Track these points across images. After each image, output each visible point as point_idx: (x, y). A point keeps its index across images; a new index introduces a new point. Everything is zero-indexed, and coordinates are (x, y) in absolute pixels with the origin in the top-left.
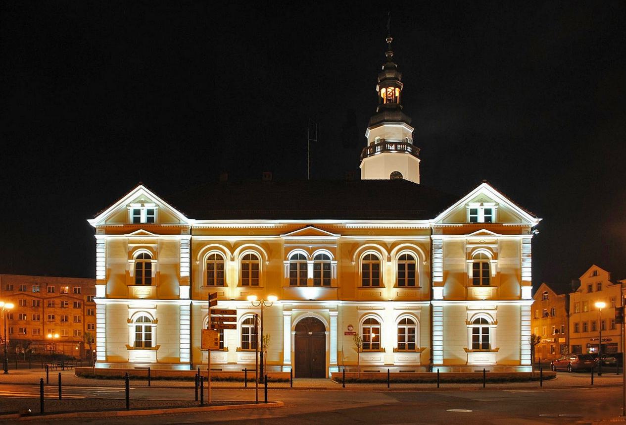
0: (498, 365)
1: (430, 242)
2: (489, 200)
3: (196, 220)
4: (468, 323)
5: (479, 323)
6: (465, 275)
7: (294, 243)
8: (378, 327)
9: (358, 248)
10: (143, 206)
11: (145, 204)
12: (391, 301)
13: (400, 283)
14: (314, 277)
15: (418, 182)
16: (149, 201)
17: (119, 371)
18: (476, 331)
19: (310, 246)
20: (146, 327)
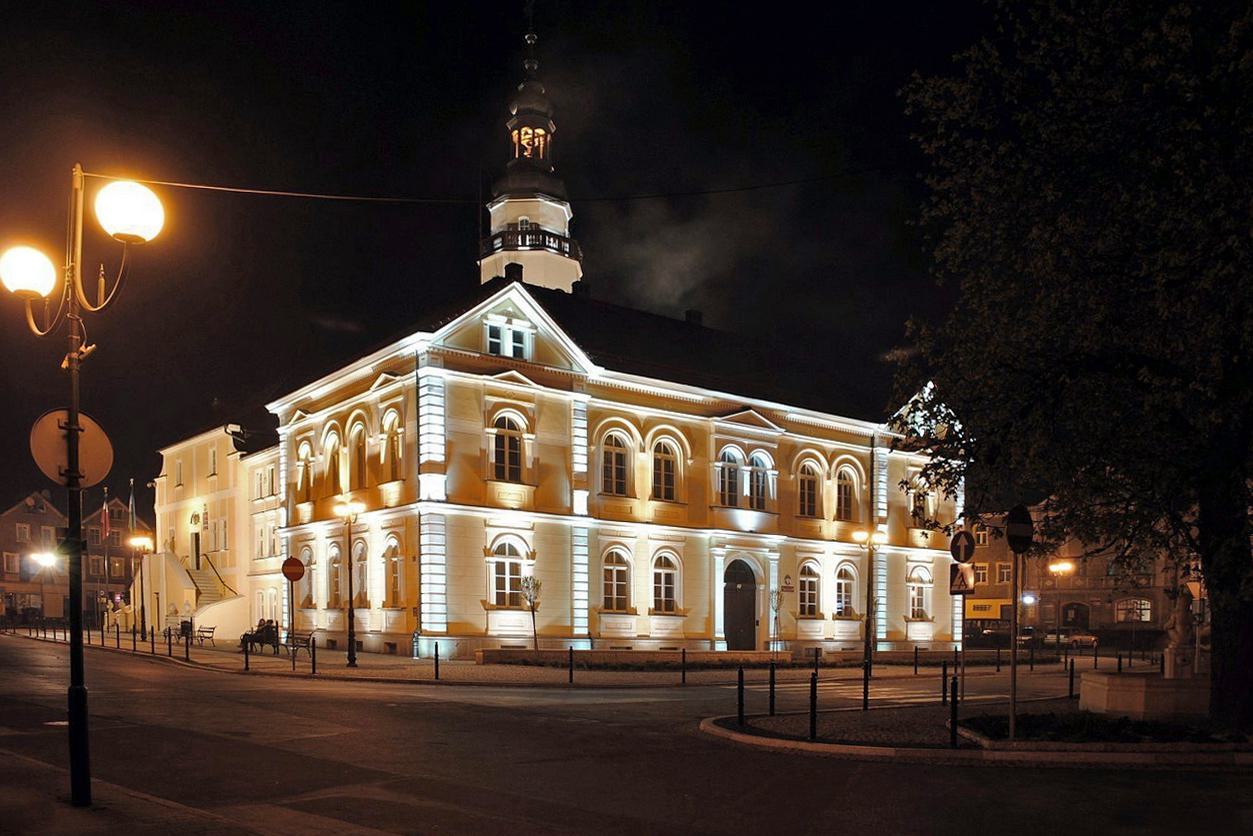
0: (934, 641)
1: (869, 456)
2: (521, 316)
3: (606, 369)
4: (487, 552)
5: (504, 554)
6: (904, 509)
7: (504, 397)
8: (624, 568)
9: (600, 421)
10: (509, 322)
11: (514, 321)
12: (647, 523)
13: (656, 495)
14: (496, 462)
15: (571, 292)
16: (521, 315)
17: (558, 654)
18: (500, 568)
19: (746, 442)
20: (511, 564)
